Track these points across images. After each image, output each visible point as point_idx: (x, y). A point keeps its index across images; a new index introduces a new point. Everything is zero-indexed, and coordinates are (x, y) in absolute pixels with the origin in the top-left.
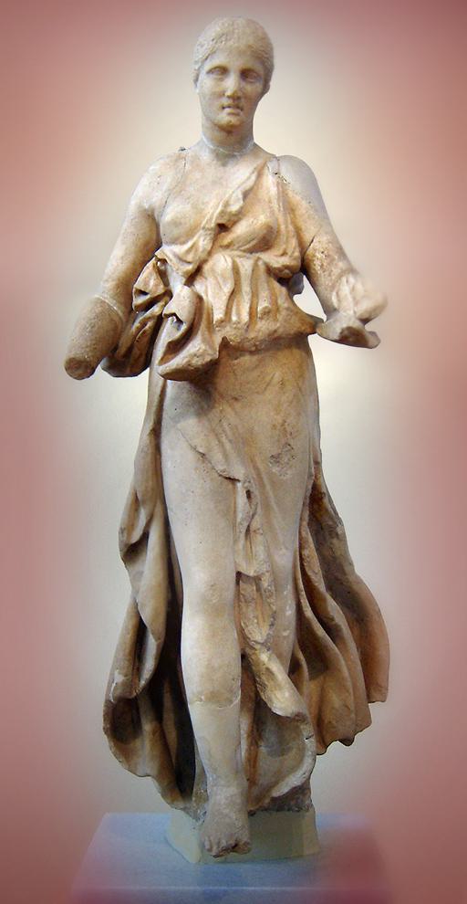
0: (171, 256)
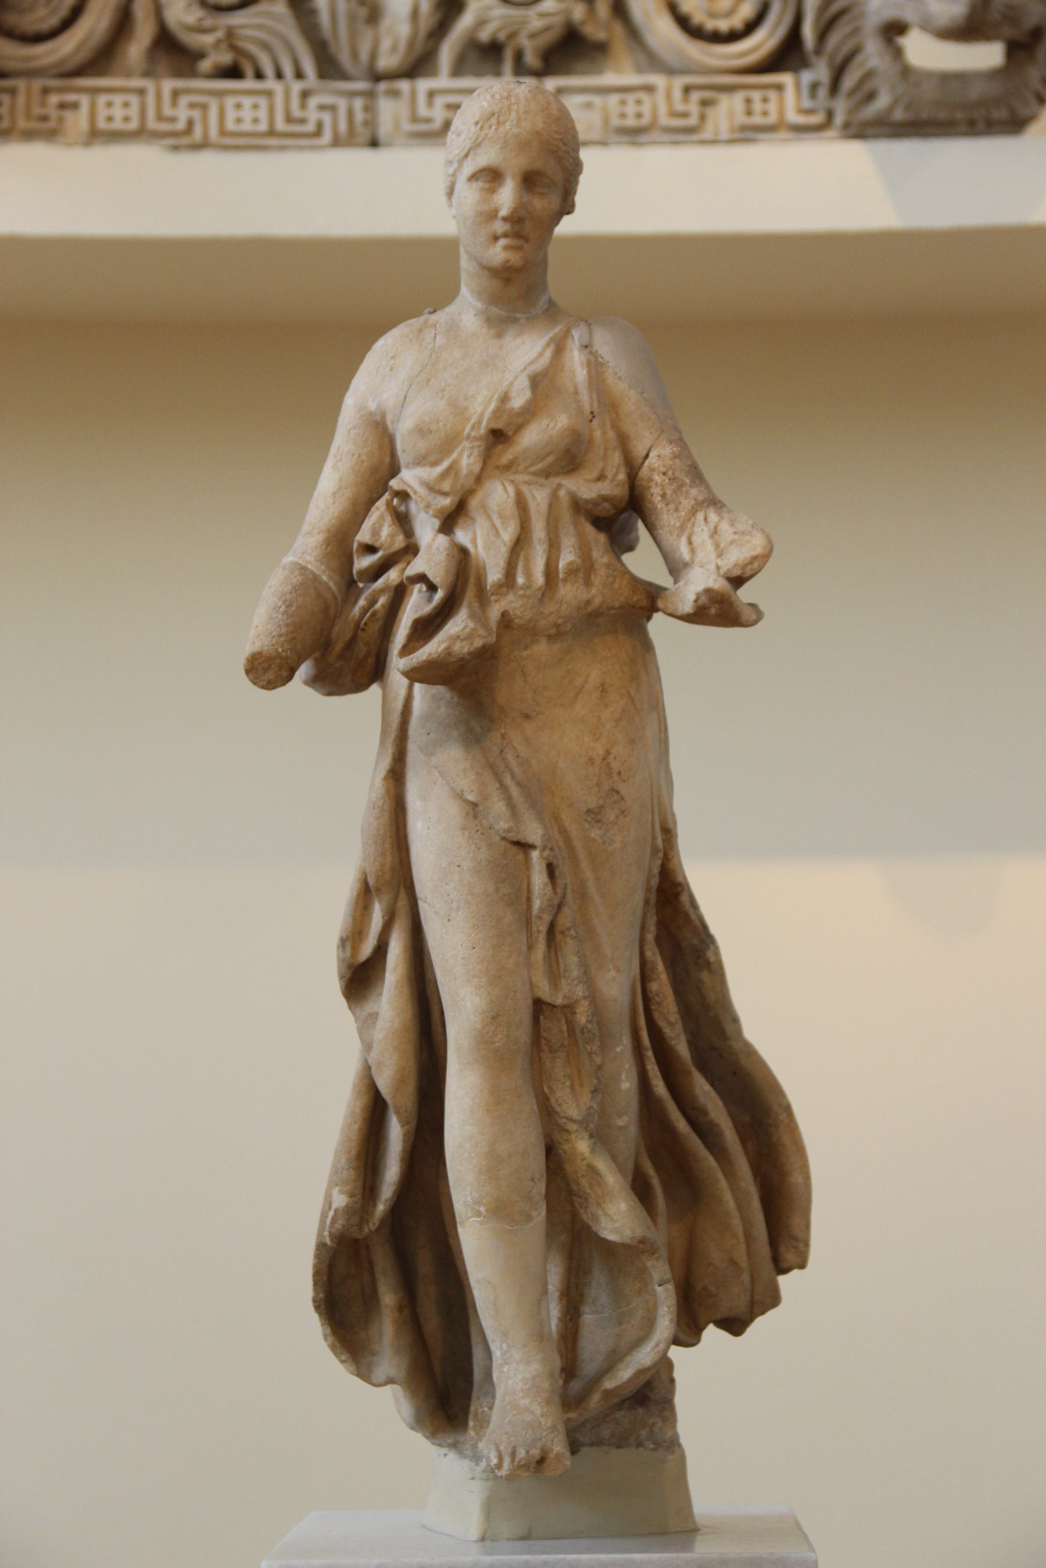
0: (416, 485)
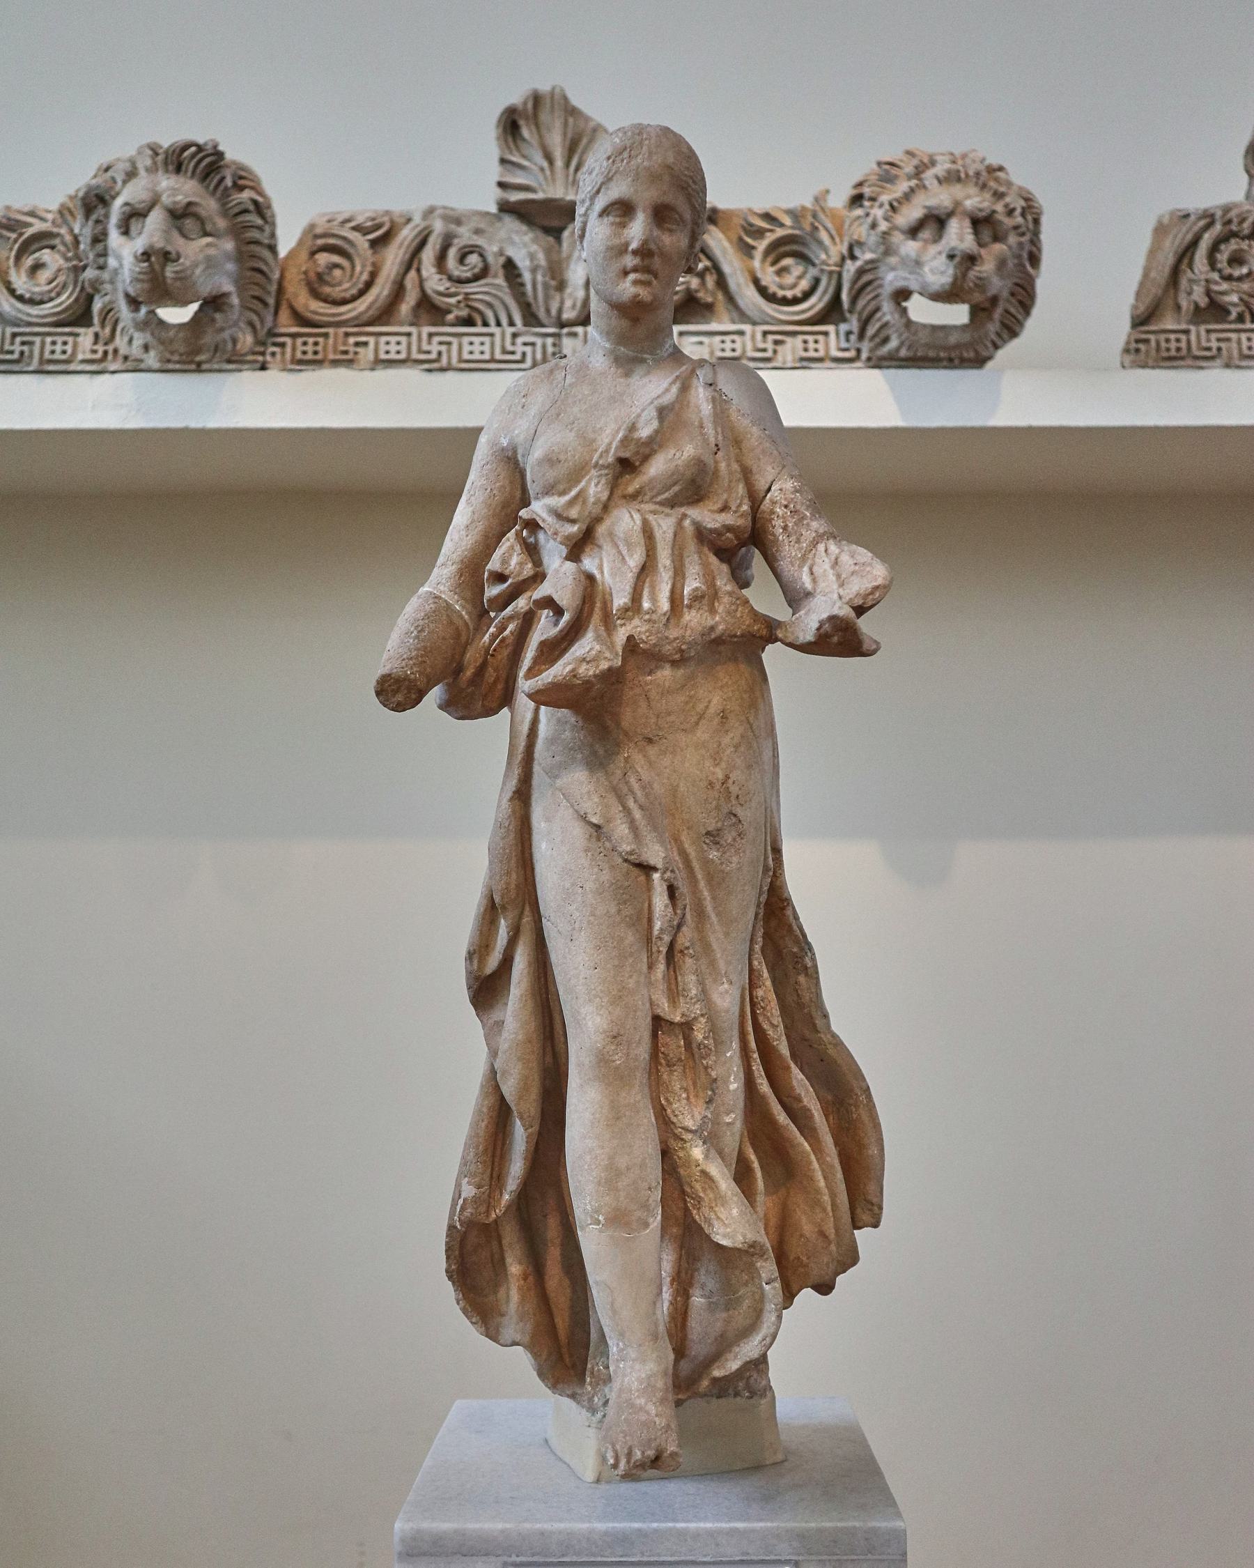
0: (545, 515)
